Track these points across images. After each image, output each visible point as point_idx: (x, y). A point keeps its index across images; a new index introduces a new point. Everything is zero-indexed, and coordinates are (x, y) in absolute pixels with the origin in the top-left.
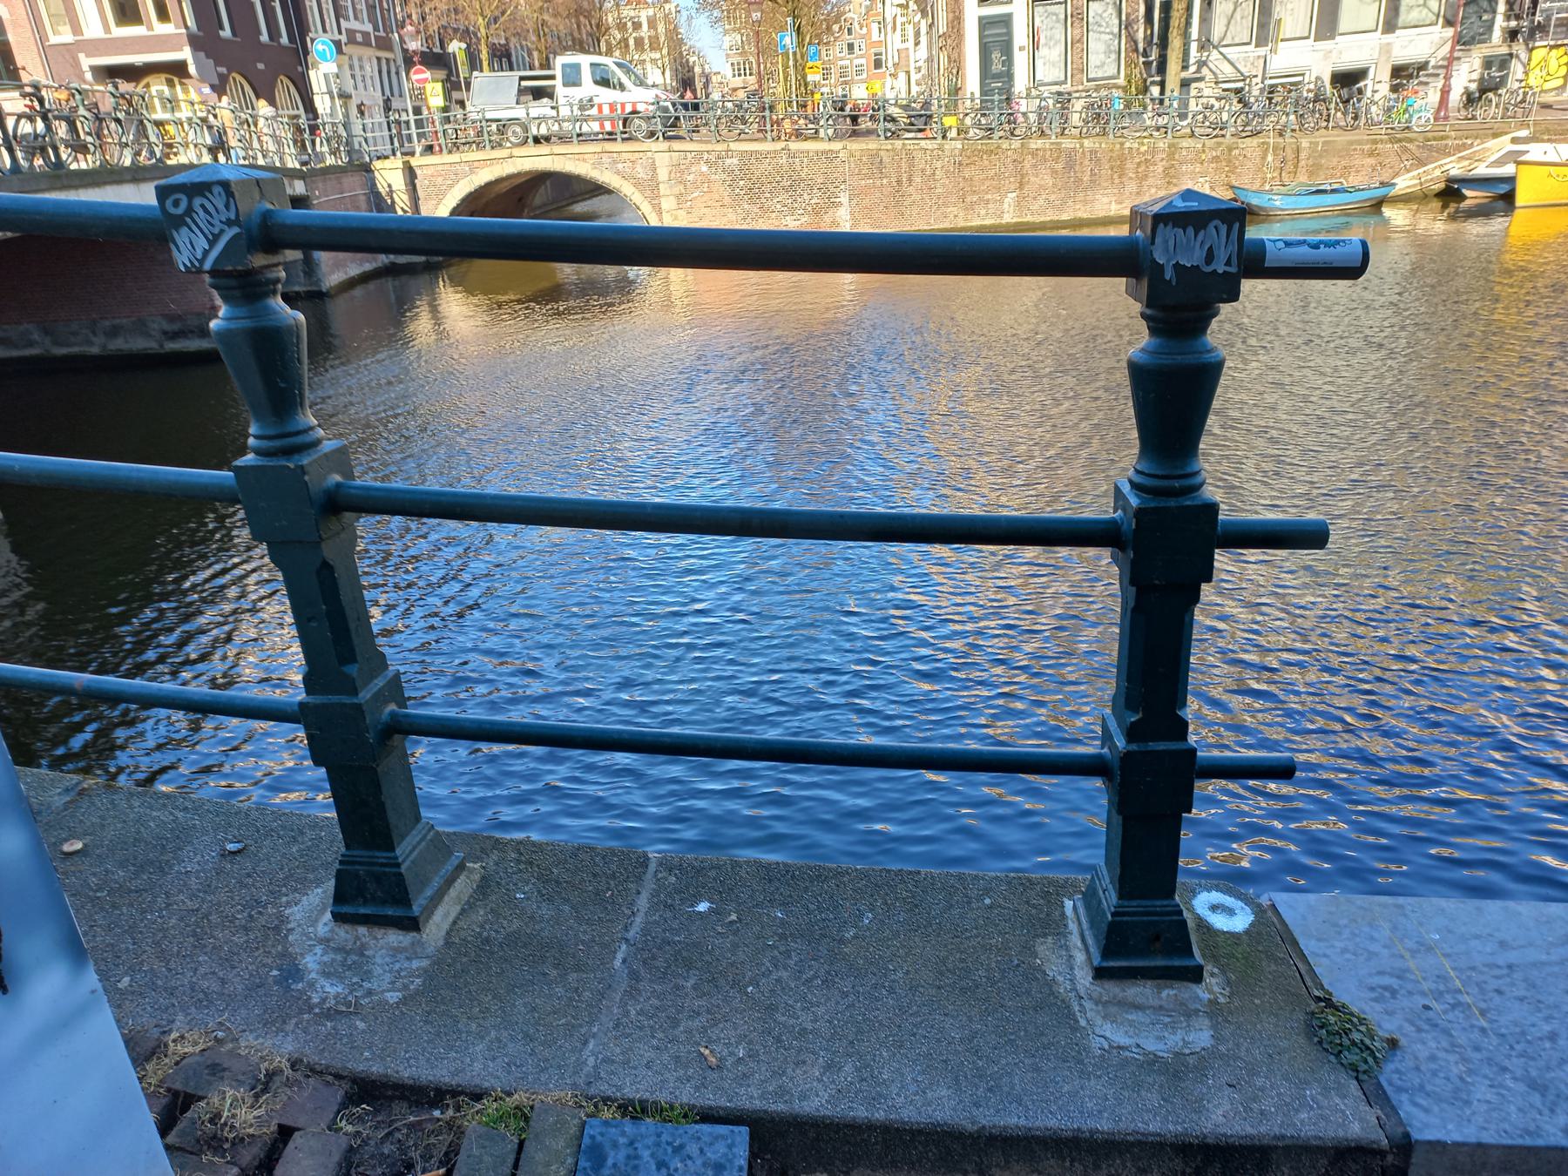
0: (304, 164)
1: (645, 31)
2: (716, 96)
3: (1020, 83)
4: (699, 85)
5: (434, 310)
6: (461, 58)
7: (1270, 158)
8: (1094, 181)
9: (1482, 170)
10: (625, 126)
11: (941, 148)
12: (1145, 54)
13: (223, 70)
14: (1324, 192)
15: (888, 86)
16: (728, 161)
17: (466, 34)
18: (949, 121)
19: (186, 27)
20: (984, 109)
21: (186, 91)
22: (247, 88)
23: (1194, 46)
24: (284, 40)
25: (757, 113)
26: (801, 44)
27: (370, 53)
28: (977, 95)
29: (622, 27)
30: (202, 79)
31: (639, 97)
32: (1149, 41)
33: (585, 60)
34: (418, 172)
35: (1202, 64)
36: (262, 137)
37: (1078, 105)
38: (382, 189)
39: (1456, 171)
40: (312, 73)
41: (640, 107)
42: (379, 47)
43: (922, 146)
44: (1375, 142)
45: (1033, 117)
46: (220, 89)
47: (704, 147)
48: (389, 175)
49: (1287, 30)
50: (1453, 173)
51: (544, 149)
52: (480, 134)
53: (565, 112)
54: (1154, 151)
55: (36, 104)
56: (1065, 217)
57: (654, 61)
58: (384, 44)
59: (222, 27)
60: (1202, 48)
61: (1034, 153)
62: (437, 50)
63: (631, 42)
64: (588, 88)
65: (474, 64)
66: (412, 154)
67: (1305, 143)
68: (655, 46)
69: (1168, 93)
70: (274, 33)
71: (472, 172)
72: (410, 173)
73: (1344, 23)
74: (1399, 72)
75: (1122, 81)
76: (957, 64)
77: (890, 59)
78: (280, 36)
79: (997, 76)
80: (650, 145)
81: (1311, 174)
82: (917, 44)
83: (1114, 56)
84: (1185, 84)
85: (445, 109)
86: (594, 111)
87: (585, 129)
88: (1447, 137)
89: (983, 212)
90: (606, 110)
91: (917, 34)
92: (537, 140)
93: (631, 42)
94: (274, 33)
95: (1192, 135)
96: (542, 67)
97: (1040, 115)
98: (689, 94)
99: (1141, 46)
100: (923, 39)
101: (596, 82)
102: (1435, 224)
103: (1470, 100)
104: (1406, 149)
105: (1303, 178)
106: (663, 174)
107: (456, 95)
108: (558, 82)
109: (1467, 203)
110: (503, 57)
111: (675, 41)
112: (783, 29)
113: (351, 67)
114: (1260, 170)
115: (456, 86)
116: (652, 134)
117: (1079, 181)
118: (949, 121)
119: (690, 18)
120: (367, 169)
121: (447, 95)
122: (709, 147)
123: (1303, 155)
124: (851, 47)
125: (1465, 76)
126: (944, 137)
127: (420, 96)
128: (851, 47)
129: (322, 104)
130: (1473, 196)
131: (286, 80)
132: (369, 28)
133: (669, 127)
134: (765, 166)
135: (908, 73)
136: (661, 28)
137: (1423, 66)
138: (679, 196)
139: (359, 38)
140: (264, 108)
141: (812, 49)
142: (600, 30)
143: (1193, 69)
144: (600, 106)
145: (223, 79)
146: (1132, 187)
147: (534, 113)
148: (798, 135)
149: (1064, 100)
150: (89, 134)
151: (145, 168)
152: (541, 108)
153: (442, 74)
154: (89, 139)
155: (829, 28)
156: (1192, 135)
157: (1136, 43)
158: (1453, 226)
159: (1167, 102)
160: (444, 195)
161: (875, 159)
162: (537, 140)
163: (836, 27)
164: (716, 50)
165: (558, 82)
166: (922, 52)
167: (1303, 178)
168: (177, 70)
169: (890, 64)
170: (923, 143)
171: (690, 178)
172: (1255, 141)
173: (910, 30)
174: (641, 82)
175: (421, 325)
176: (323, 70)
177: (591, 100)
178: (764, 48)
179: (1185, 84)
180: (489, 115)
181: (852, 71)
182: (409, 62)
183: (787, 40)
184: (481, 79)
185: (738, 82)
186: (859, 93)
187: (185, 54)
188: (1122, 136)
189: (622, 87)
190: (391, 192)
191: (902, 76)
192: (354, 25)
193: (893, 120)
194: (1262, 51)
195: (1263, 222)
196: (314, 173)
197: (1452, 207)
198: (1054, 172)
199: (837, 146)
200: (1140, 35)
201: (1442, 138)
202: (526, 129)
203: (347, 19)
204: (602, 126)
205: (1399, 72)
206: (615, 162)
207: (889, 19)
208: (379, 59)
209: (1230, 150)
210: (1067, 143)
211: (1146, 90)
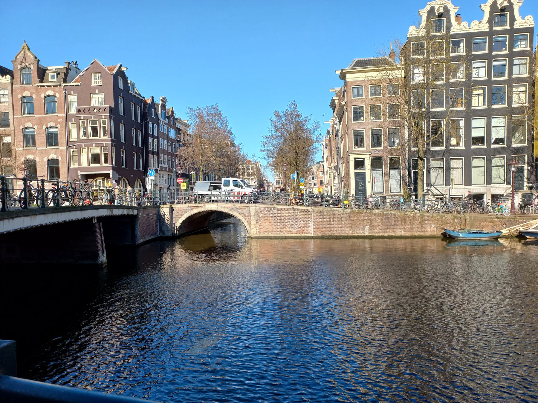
0: (139, 204)
1: (250, 170)
2: (270, 189)
3: (369, 193)
4: (265, 186)
5: (172, 251)
6: (193, 176)
7: (456, 221)
8: (396, 225)
9: (531, 230)
10: (242, 198)
11: (344, 211)
12: (409, 186)
13: (121, 177)
14: (477, 233)
15: (324, 190)
17: (197, 170)
18: (346, 202)
19: (112, 164)
20: (357, 199)
21: (108, 182)
22: (140, 182)
23: (425, 185)
24: (141, 169)
25: (282, 197)
26: (298, 177)
27: (167, 173)
28: (355, 195)
29: (243, 169)
30: (113, 179)
31: (247, 190)
32: (410, 183)
33: (231, 179)
34: (174, 209)
35: (428, 190)
36: (127, 197)
37: (388, 201)
38: (162, 213)
39: (522, 229)
40: (147, 178)
41: (247, 193)
42: (169, 172)
43: (339, 210)
44: (492, 218)
45: (374, 203)
46: (118, 182)
47: (266, 206)
48: (165, 210)
49: (455, 182)
50: (521, 230)
51: (215, 204)
52: (195, 199)
53: (223, 193)
54: (416, 216)
55: (56, 187)
56: (386, 235)
57: (252, 179)
58: (171, 171)
59: (123, 165)
60: (428, 185)
61: (375, 214)
62: (187, 173)
63: (246, 174)
64: (231, 187)
65: (197, 178)
66: (173, 203)
67: (467, 217)
68: (253, 174)
69: (419, 198)
70: (138, 167)
71: (191, 210)
72: (172, 209)
73: (474, 181)
74: (493, 196)
75: (402, 193)
76: (348, 186)
77: (326, 182)
78: (140, 168)
79: (361, 190)
80: (250, 205)
81: (471, 227)
82: (334, 179)
83: (399, 186)
84: (424, 195)
85: (187, 190)
86: (233, 194)
87: (229, 199)
88: (516, 219)
89: (358, 231)
90: (236, 193)
91: (334, 176)
92: (213, 201)
93: (246, 174)
94: (138, 167)
95: (428, 211)
96: (218, 180)
97: (376, 203)
98: (262, 189)
99: (408, 184)
100: (336, 178)
101: (234, 185)
102: (519, 247)
103: (521, 207)
104: (503, 222)
105: (468, 228)
106: (252, 214)
107: (190, 186)
108: (222, 185)
109: (528, 240)
110: (206, 177)
111: (259, 173)
112: (293, 173)
113: (160, 177)
114: (453, 224)
115: (191, 183)
116: (250, 201)
117: (390, 224)
118: (346, 202)
119: (264, 168)
120: (159, 207)
121: (188, 186)
122: (268, 206)
123: (467, 220)
124: (313, 178)
125: (518, 199)
126: (344, 207)
127: (179, 185)
128: (313, 178)
129: (148, 187)
130: (530, 238)
131: (139, 180)
132: (167, 166)
133: (256, 200)
135: (331, 187)
136: (255, 170)
137: (502, 195)
138: (257, 221)
139: (164, 169)
140: (129, 189)
141: (302, 179)
142: (237, 170)
143: (425, 191)
144: (234, 193)
145: (120, 179)
146: (408, 227)
147: (213, 193)
148: (297, 204)
149: (384, 198)
150: (71, 196)
151: (85, 206)
152: (216, 192)
153: (187, 180)
154: (70, 197)
155: (306, 173)
156: (428, 211)
157: (406, 183)
158: (525, 247)
159: (419, 201)
160: (181, 216)
161: (322, 213)
162: (213, 201)
163: (308, 173)
164: (272, 177)
165: (222, 185)
166: (336, 181)
167: (468, 228)
168: (107, 176)
169: (325, 183)
170: (338, 209)
171: (261, 215)
172: (450, 215)
173: (332, 175)
174: (248, 186)
175: (167, 258)
176: (150, 179)
177: (232, 190)
178: (286, 177)
179: (424, 195)
180: (199, 193)
181: (313, 184)
182: (177, 176)
183: (294, 176)
184: (198, 183)
185: (277, 186)
186: (315, 191)
187: (110, 172)
188: (404, 211)
189: (242, 187)
190: (165, 214)
191: (329, 187)
192: (163, 165)
193: (328, 201)
194: (448, 187)
195: (456, 241)
196: (141, 208)
197: (523, 241)
198: (382, 220)
199: (309, 208)
200: (407, 180)
201: (515, 219)
202: (210, 198)
203: (161, 164)
204: (234, 198)
205: (493, 196)
207: (325, 171)
209: (442, 217)
210: (386, 212)
211: (410, 196)
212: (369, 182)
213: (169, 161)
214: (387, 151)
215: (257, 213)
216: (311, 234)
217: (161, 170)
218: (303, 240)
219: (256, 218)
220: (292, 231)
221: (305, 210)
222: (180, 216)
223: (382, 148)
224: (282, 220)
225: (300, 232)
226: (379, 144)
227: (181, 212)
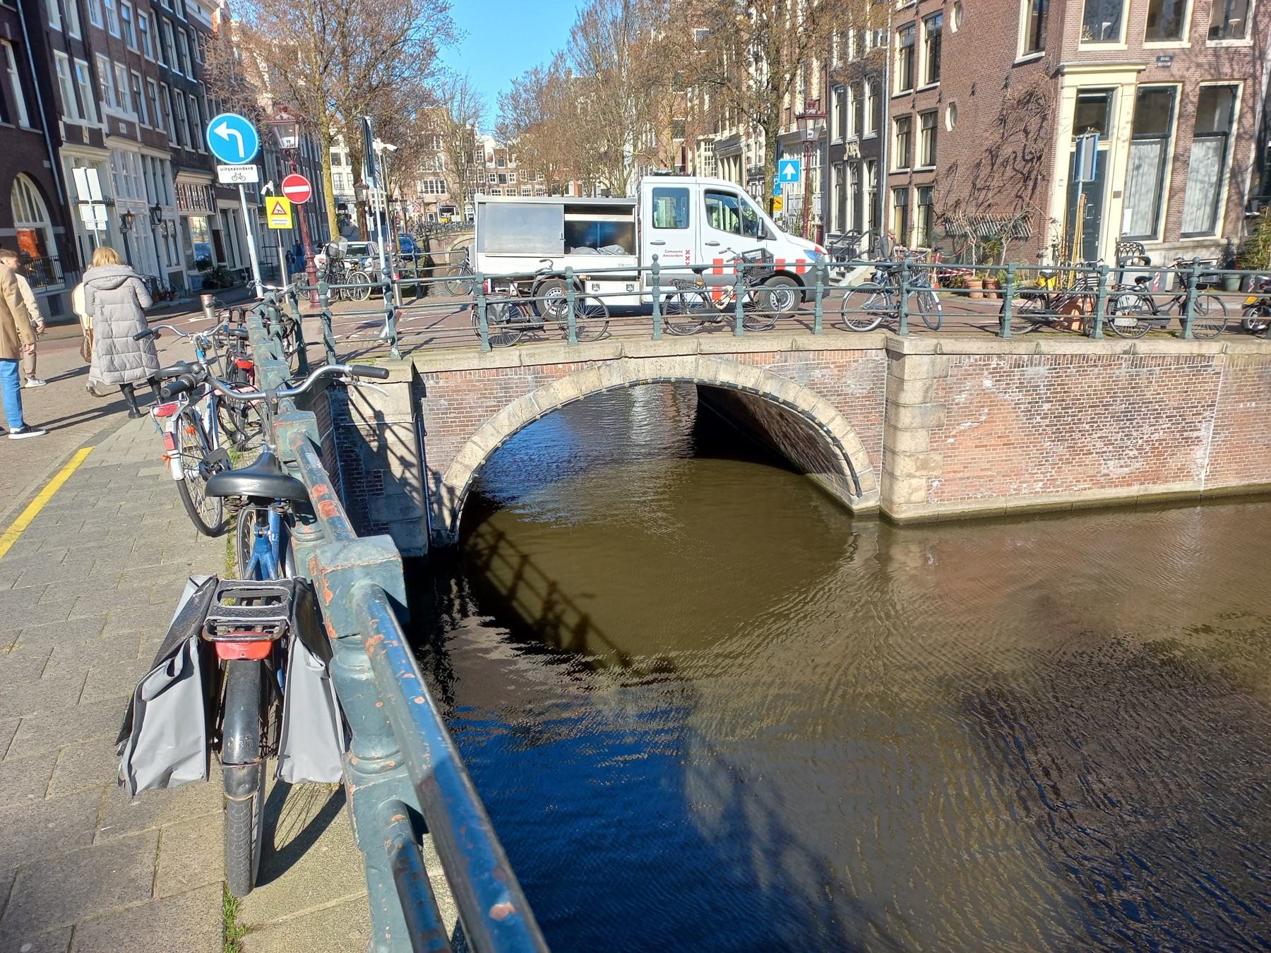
16: (1030, 371)
22: (34, 192)
34: (429, 383)
78: (17, 117)
131: (23, 178)
132: (133, 117)
134: (1093, 380)
138: (936, 431)
139: (123, 129)
157: (1241, 195)
171: (962, 398)
190: (381, 423)
206: (808, 368)
208: (143, 156)
212: (1117, 195)
213: (135, 95)
214: (1201, 59)
215: (942, 385)
216: (1198, 483)
217: (114, 132)
218: (1152, 516)
219: (932, 420)
220: (1110, 476)
221: (1190, 358)
222: (469, 426)
223: (1185, 44)
224: (1063, 419)
225: (1143, 477)
226: (1174, 32)
227: (471, 398)
